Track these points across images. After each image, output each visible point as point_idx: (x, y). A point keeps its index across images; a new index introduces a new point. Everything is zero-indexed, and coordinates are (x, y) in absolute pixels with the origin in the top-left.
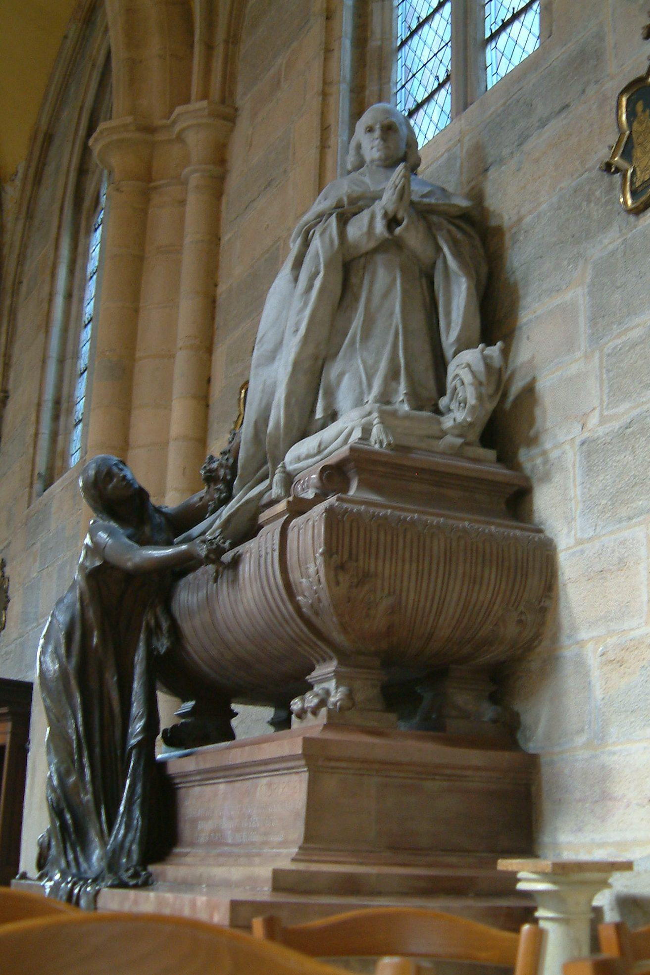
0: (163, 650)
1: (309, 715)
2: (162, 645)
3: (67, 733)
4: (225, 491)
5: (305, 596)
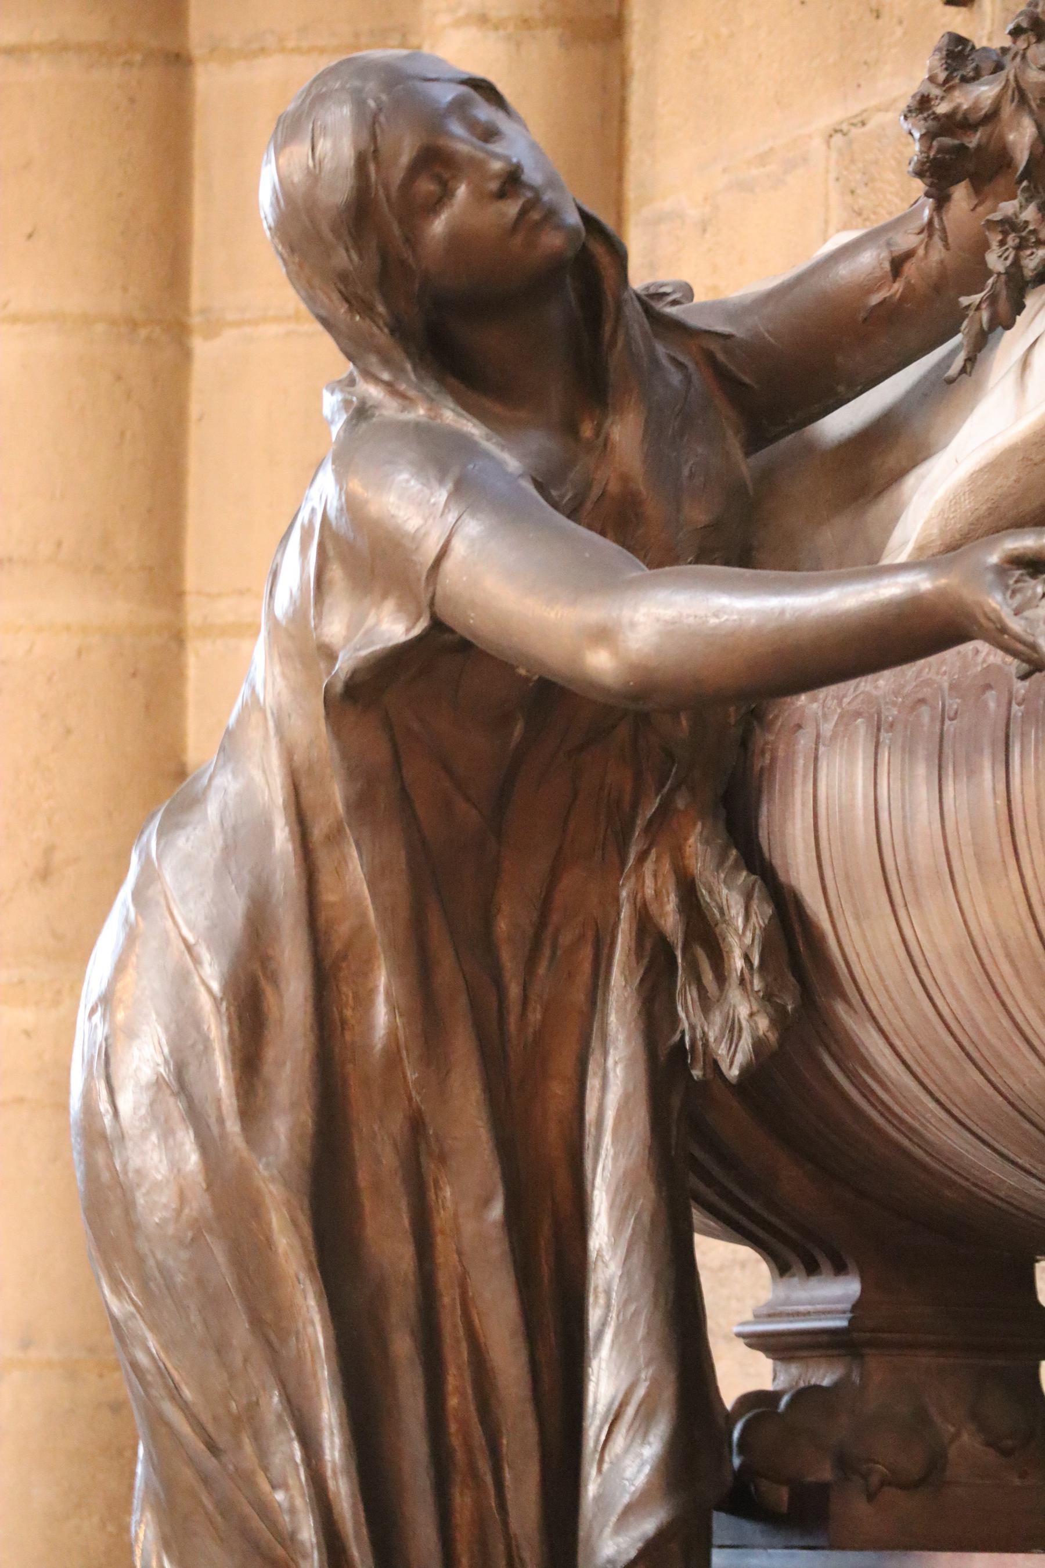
2: (732, 1028)
3: (265, 1510)
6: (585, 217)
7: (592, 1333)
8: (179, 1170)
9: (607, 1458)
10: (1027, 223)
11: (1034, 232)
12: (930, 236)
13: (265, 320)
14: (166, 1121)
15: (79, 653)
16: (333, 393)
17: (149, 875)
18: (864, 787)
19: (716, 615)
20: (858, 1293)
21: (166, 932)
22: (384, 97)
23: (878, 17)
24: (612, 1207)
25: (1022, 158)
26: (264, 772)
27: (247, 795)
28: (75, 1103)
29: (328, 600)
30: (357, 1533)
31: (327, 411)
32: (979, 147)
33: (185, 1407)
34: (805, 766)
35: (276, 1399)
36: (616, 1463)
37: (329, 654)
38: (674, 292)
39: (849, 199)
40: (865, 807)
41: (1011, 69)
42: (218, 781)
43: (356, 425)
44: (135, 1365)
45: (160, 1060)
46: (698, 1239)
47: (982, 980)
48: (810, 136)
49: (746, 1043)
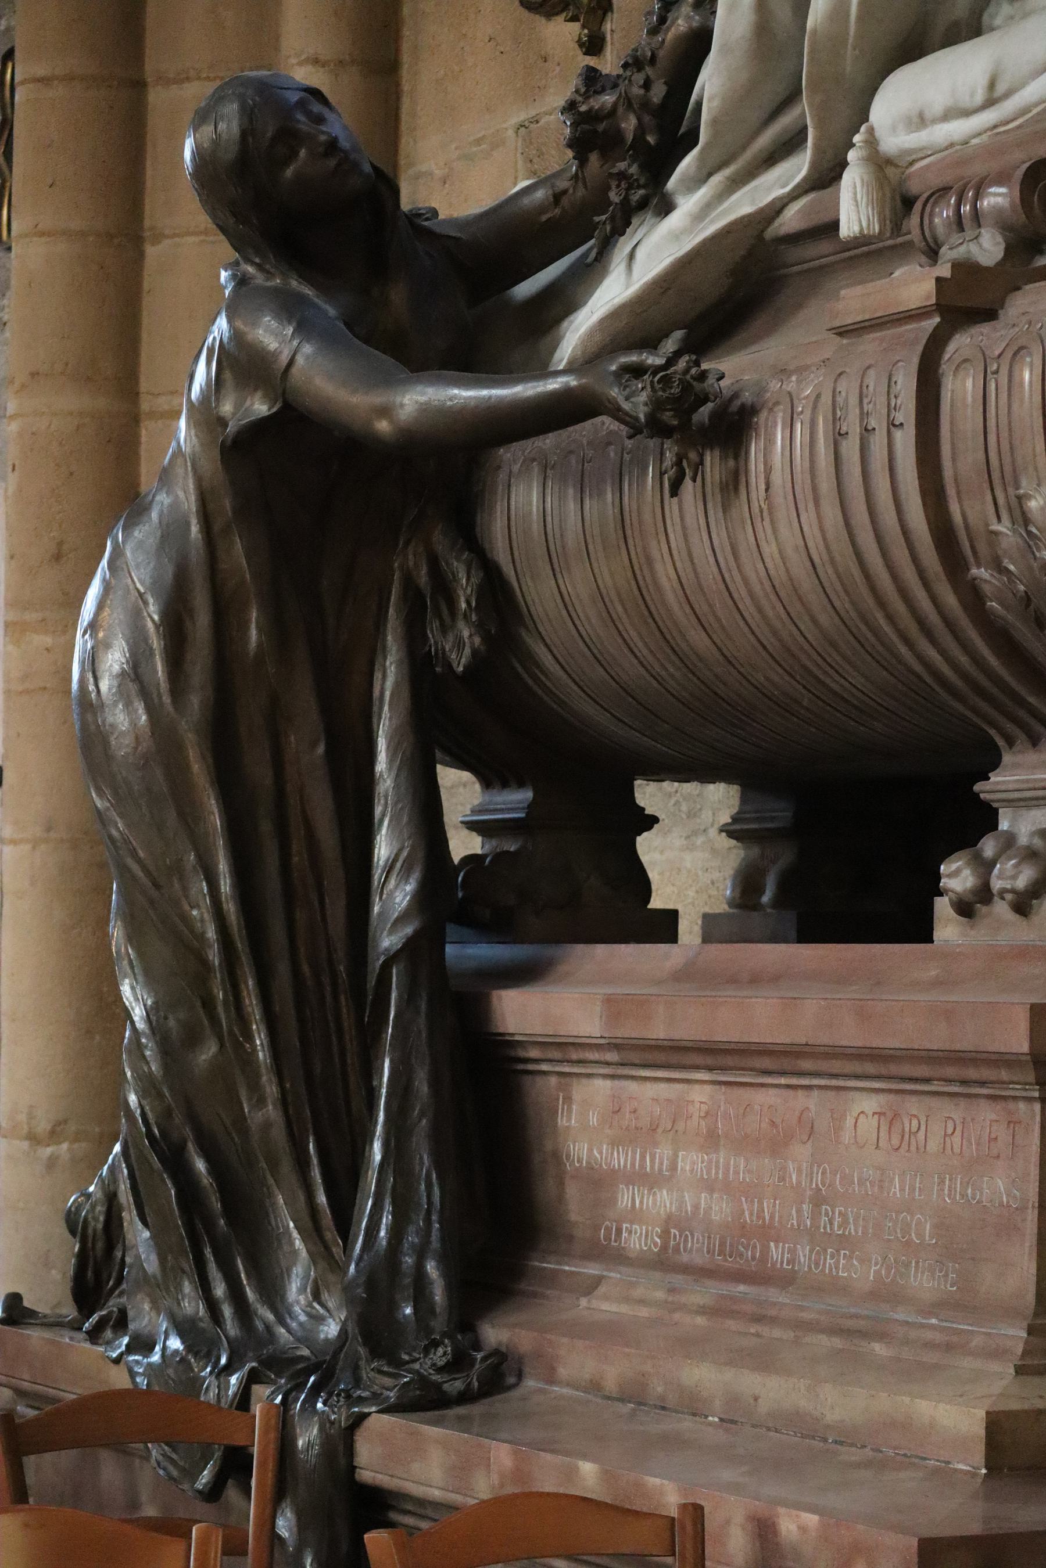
0: (460, 663)
1: (1001, 909)
2: (459, 644)
3: (185, 918)
4: (642, 181)
5: (1001, 570)
6: (375, 168)
7: (376, 820)
8: (135, 725)
9: (385, 892)
10: (632, 175)
11: (637, 180)
12: (576, 182)
13: (189, 234)
14: (128, 696)
15: (78, 427)
16: (226, 271)
17: (117, 553)
18: (537, 501)
19: (451, 400)
20: (531, 799)
21: (128, 586)
22: (257, 99)
23: (545, 61)
24: (388, 748)
25: (630, 137)
26: (185, 492)
27: (175, 505)
28: (75, 685)
29: (223, 392)
30: (239, 930)
31: (223, 279)
32: (605, 132)
33: (139, 861)
34: (503, 490)
35: (192, 857)
36: (391, 894)
37: (223, 422)
38: (427, 213)
39: (529, 165)
40: (538, 514)
41: (622, 88)
42: (158, 498)
43: (240, 289)
44: (111, 837)
45: (124, 660)
46: (439, 767)
47: (605, 614)
48: (506, 129)
49: (467, 651)
